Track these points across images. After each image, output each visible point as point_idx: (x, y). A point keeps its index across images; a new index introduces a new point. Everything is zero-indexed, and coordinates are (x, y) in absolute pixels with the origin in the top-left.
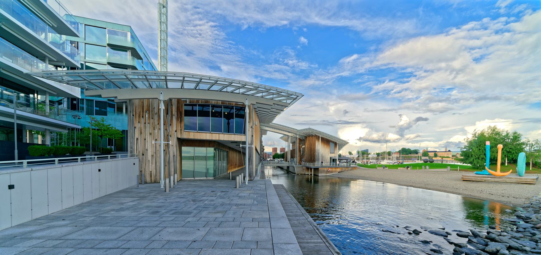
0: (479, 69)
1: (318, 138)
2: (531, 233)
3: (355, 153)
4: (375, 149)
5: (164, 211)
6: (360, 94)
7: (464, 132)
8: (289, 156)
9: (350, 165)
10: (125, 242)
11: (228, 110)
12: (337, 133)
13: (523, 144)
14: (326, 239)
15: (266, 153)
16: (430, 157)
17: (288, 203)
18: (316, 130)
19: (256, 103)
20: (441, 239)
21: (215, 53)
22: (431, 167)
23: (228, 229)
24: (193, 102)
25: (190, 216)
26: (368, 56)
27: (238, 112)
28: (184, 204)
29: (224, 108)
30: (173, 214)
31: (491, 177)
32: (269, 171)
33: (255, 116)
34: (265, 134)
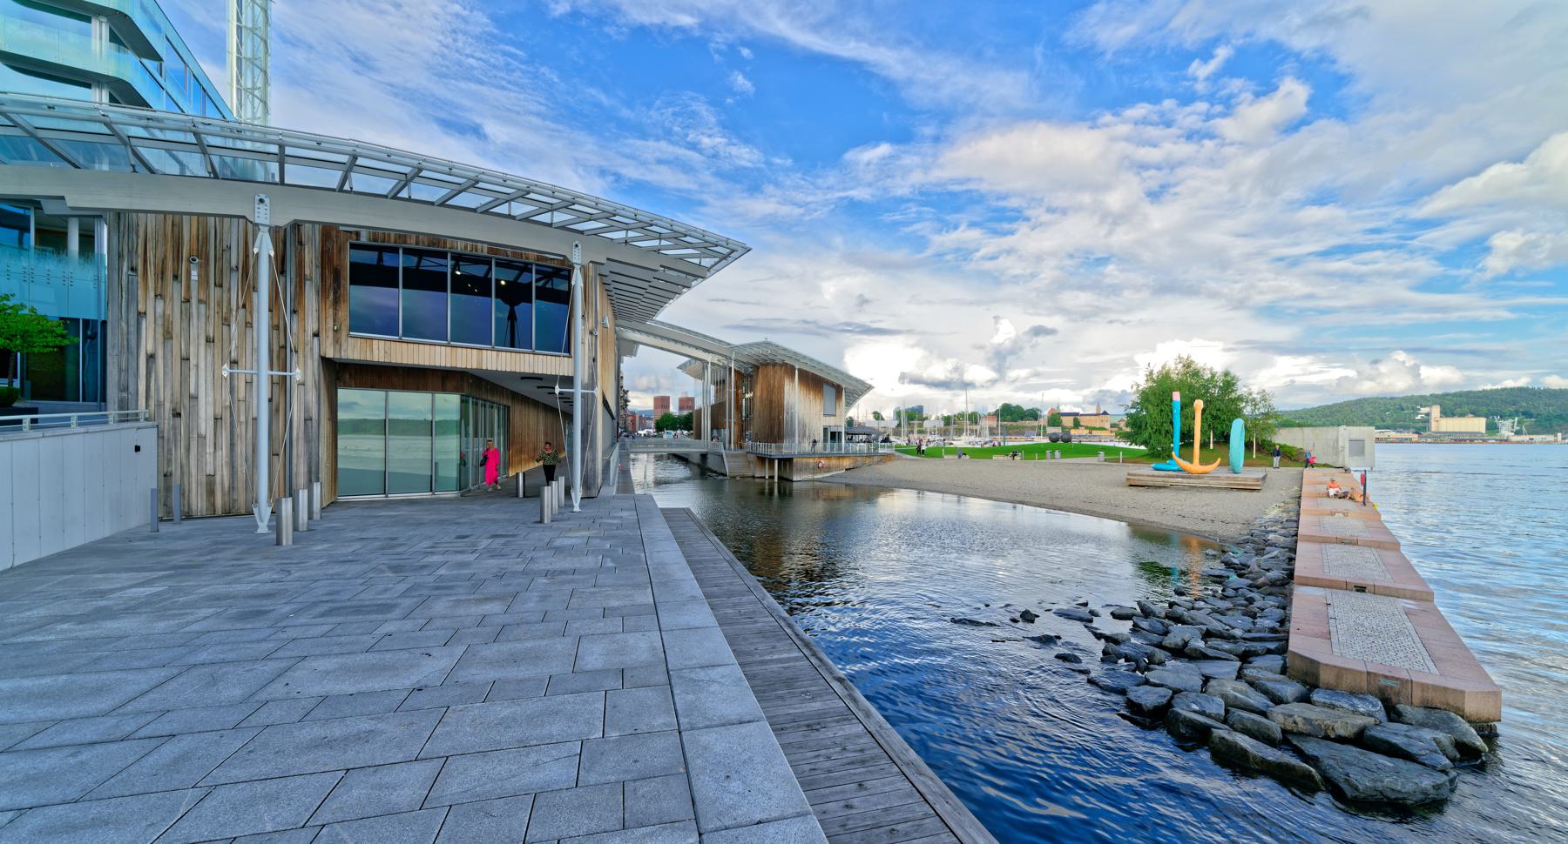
0: (1160, 218)
1: (790, 370)
2: (1246, 599)
3: (888, 414)
4: (941, 405)
5: (287, 608)
6: (900, 255)
7: (1131, 363)
8: (706, 423)
9: (876, 449)
10: (149, 717)
11: (511, 275)
12: (842, 357)
13: (1240, 399)
14: (811, 650)
15: (633, 414)
16: (1065, 428)
17: (706, 561)
18: (785, 349)
19: (608, 259)
20: (1079, 626)
21: (456, 79)
22: (1065, 454)
23: (529, 644)
24: (386, 237)
25: (389, 616)
26: (916, 154)
27: (546, 283)
28: (361, 581)
29: (498, 265)
30: (323, 615)
31: (1182, 477)
32: (643, 470)
33: (602, 303)
34: (632, 353)
